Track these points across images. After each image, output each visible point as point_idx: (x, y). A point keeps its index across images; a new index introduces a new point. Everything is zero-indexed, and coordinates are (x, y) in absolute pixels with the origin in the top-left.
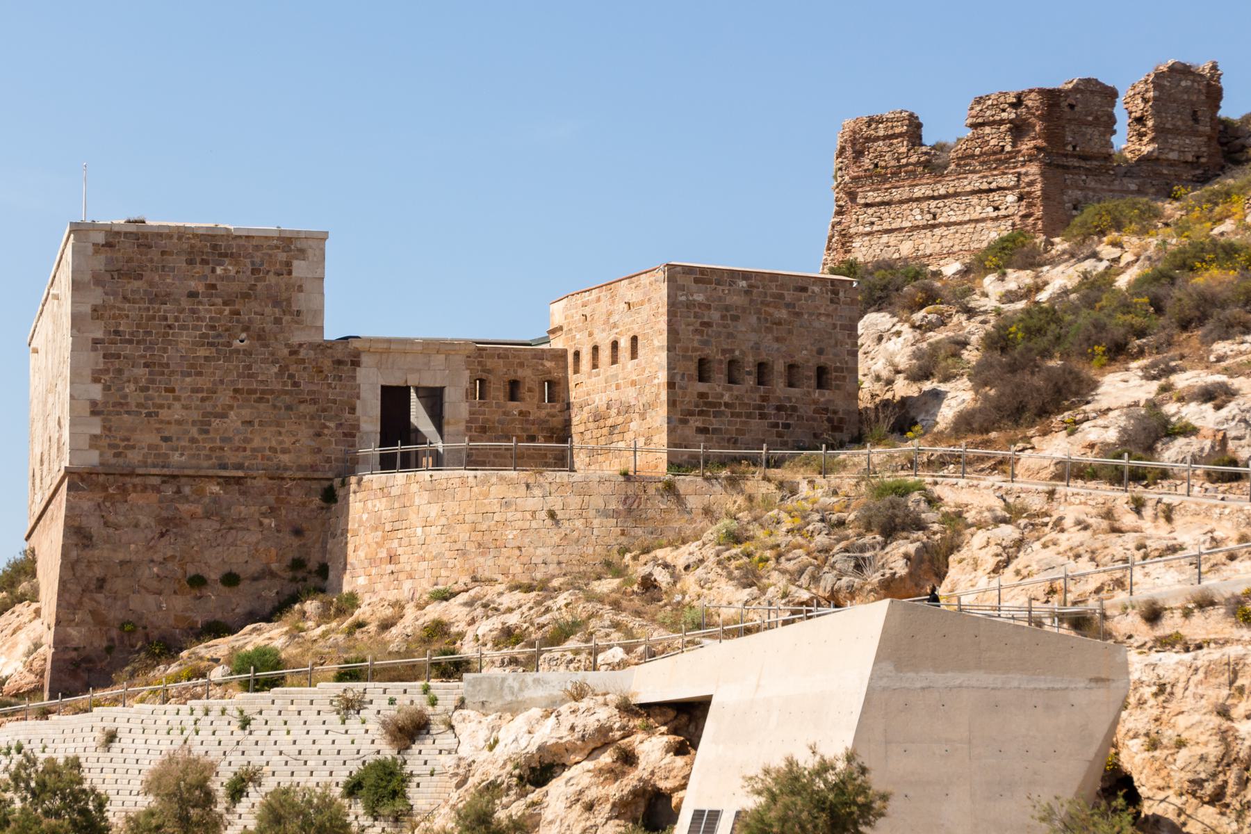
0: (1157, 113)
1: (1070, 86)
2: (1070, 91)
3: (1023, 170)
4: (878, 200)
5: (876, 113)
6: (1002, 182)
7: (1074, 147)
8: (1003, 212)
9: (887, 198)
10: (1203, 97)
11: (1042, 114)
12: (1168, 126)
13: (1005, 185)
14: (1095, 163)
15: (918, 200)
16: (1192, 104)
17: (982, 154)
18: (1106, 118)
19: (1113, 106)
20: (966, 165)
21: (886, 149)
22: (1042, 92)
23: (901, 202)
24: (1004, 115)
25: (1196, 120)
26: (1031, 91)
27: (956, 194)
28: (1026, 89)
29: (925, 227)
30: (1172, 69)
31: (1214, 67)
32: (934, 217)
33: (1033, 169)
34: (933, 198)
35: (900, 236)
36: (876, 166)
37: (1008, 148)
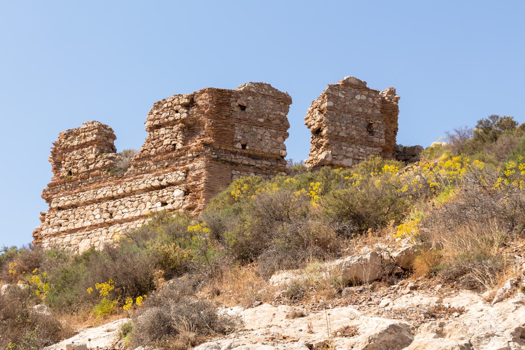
0: (332, 122)
1: (242, 89)
2: (241, 92)
3: (190, 166)
4: (67, 203)
5: (73, 126)
6: (172, 178)
7: (244, 146)
8: (169, 206)
9: (74, 202)
10: (378, 112)
11: (210, 112)
12: (342, 134)
13: (173, 180)
14: (265, 162)
15: (100, 201)
16: (367, 117)
17: (157, 153)
18: (278, 121)
19: (287, 111)
20: (142, 165)
21: (79, 157)
22: (212, 91)
23: (86, 204)
24: (177, 116)
25: (371, 133)
26: (203, 92)
27: (133, 193)
28: (198, 91)
29: (102, 225)
30: (346, 83)
31: (392, 92)
32: (111, 216)
33: (200, 163)
34: (113, 198)
35: (80, 234)
36: (70, 173)
37: (179, 146)
